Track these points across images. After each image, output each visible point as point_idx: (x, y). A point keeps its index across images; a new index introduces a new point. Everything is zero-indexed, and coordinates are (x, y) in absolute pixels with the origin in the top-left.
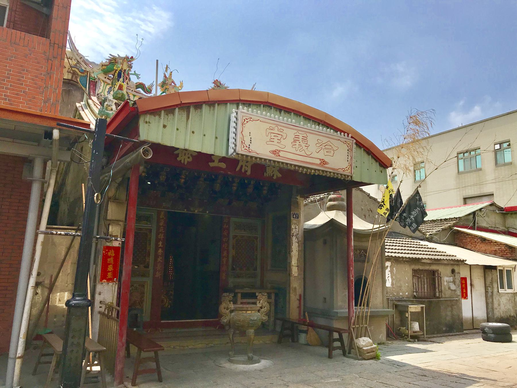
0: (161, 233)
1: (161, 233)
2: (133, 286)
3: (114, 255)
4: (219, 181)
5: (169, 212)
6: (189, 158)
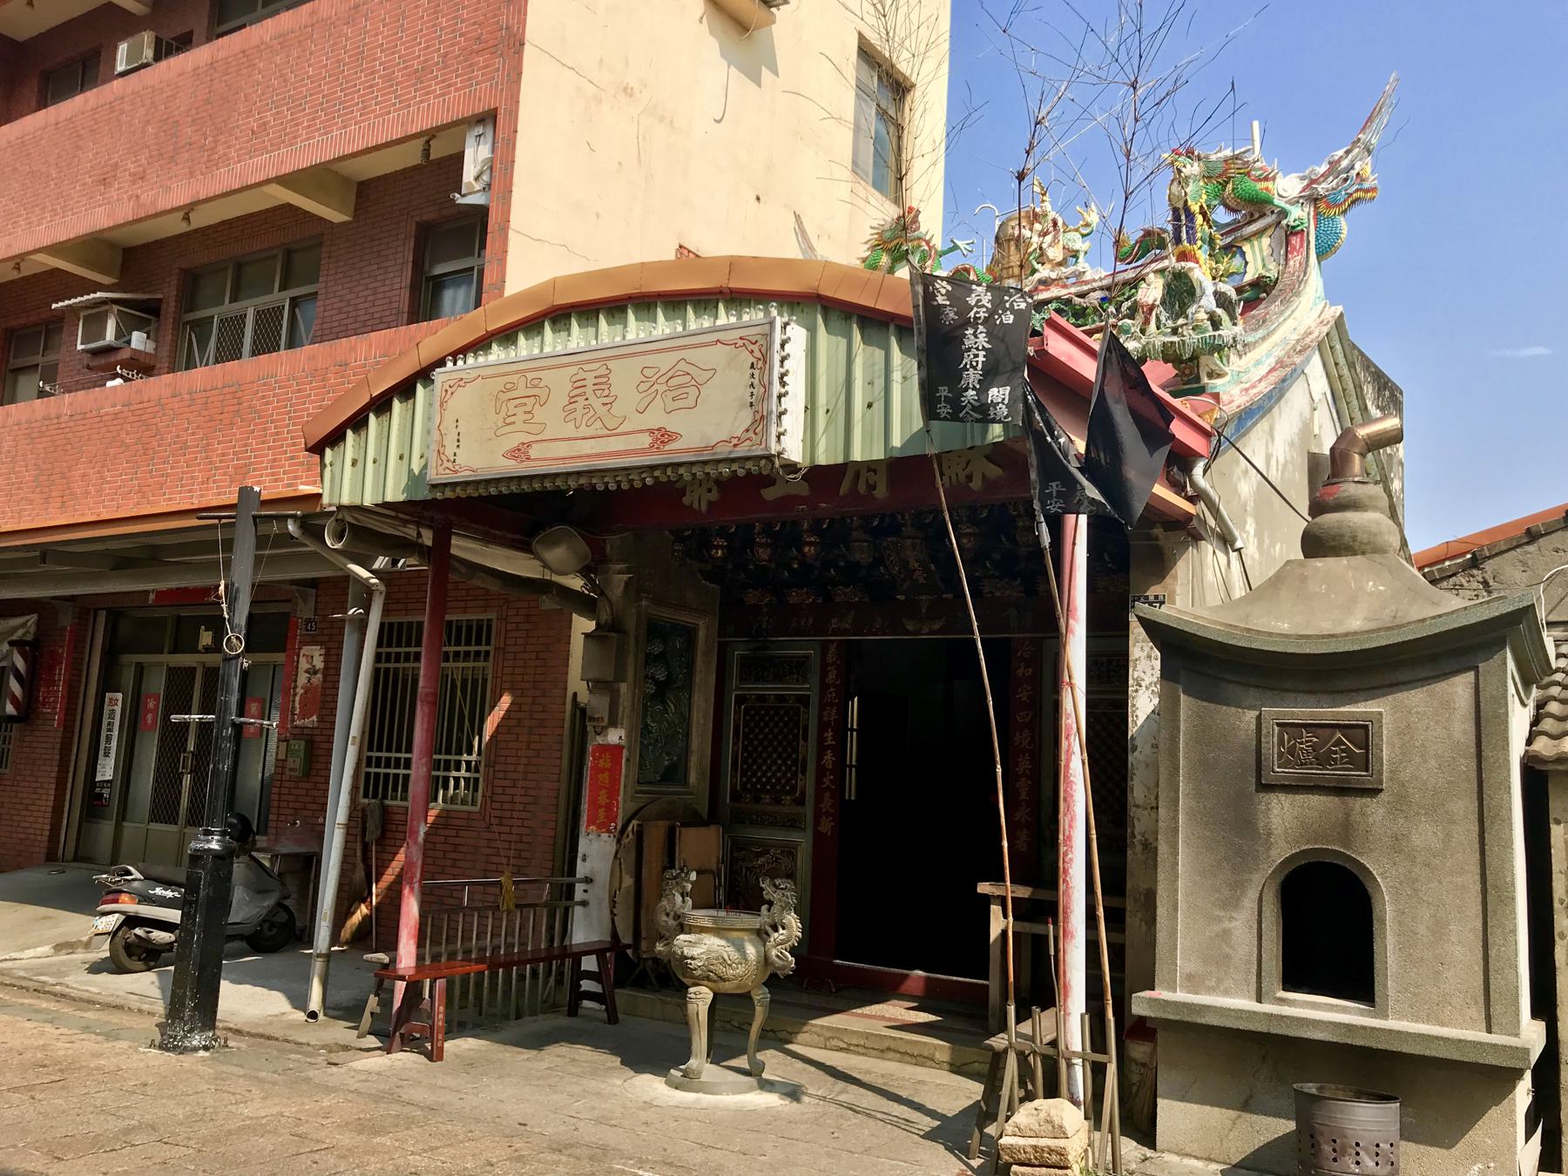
0: (831, 704)
1: (831, 704)
3: (608, 765)
6: (709, 491)
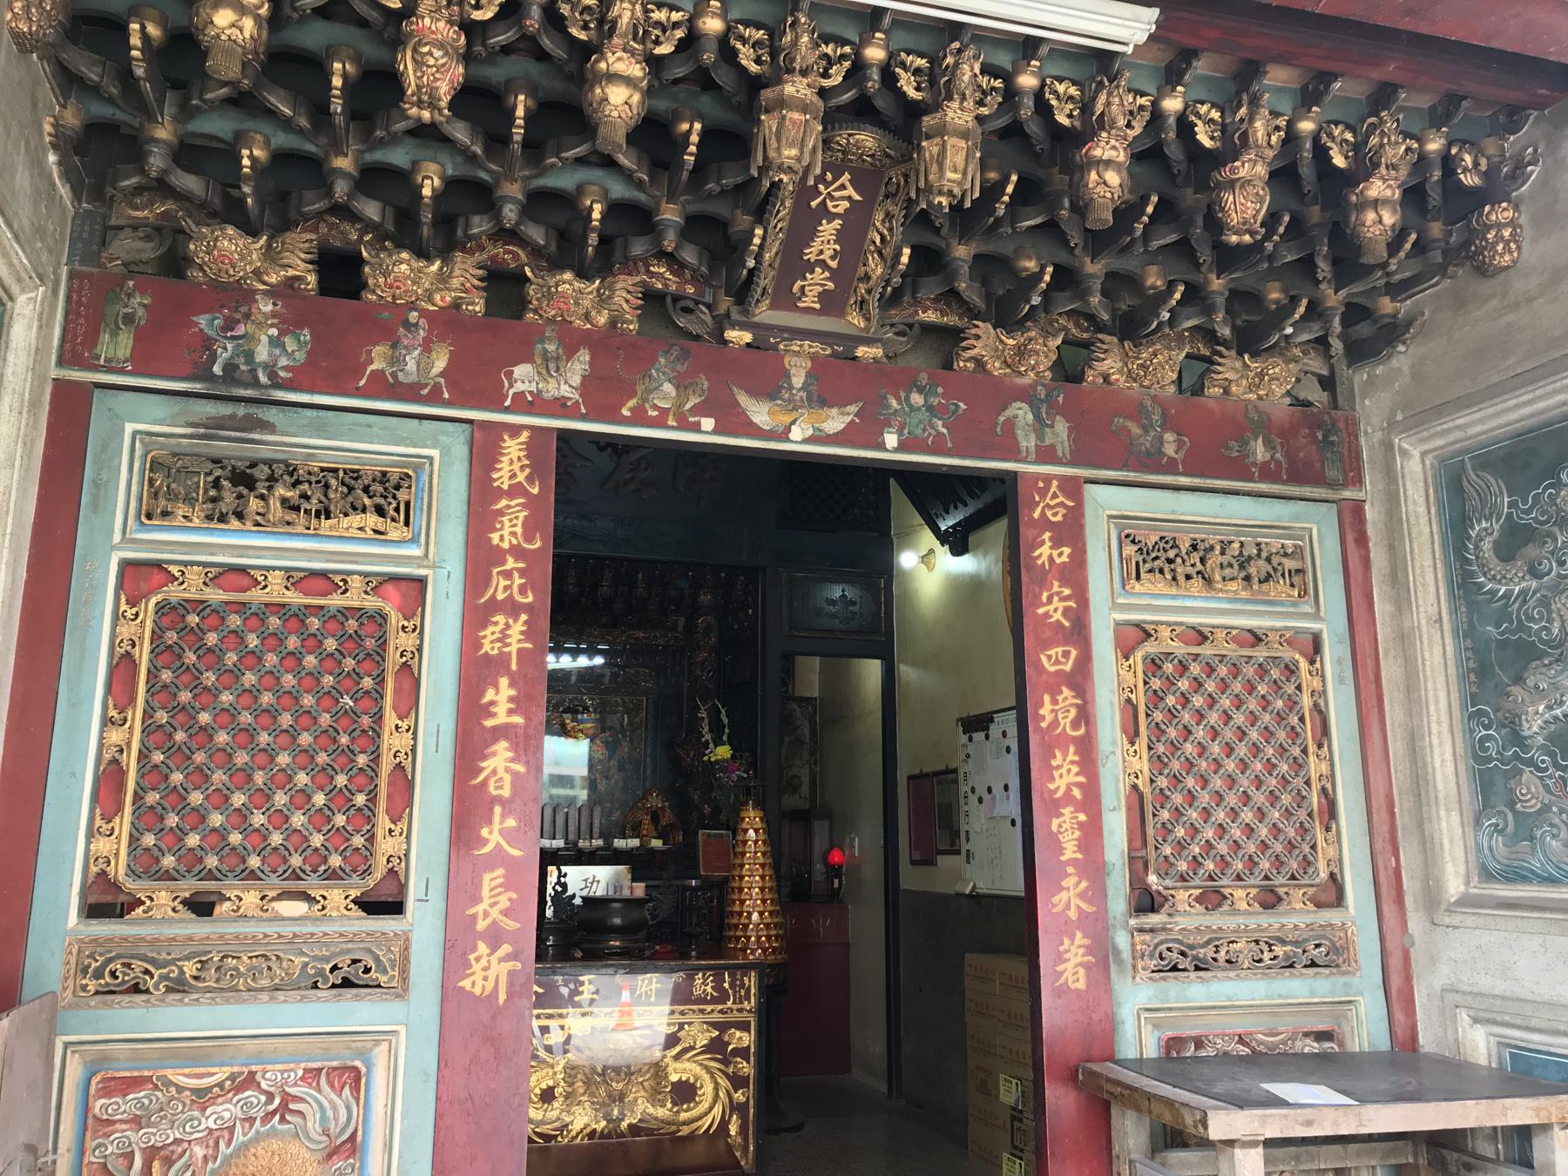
2: (250, 1081)
4: (958, 114)
5: (564, 436)
